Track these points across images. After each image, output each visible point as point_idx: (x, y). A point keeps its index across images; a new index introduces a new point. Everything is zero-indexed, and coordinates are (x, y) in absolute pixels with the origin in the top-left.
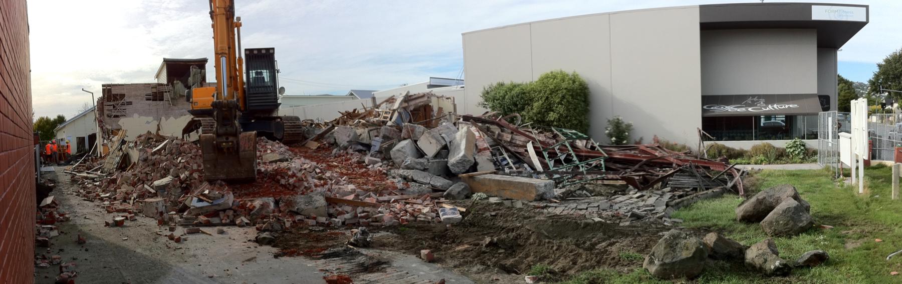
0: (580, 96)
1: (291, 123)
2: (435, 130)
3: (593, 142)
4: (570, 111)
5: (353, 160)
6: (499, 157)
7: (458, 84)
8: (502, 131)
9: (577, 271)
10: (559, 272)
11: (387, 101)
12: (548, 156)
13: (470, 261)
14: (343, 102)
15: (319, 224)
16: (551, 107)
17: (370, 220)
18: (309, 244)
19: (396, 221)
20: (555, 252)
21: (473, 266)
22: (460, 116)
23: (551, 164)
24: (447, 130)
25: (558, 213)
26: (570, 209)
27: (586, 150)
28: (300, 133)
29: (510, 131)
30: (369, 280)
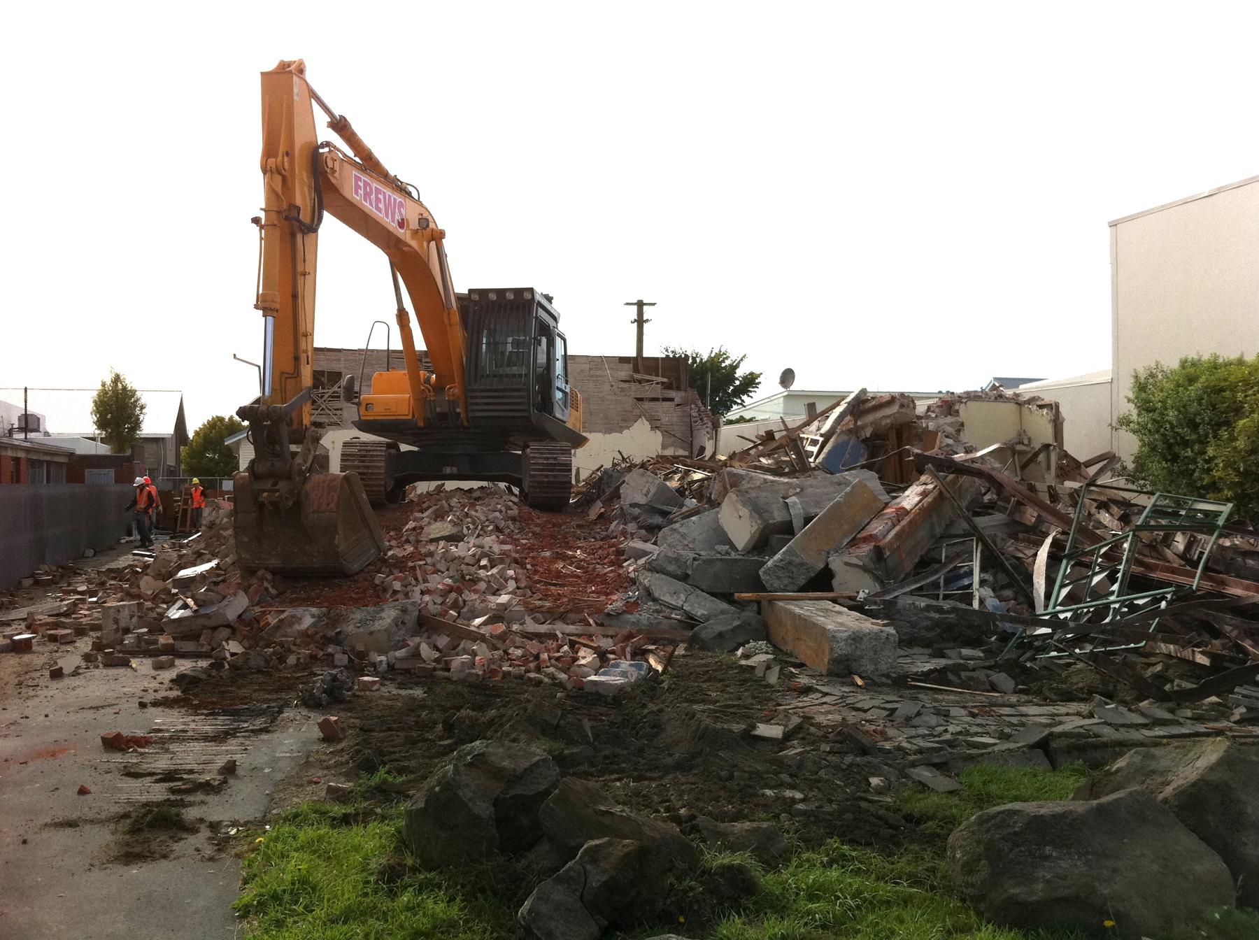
1: (545, 459)
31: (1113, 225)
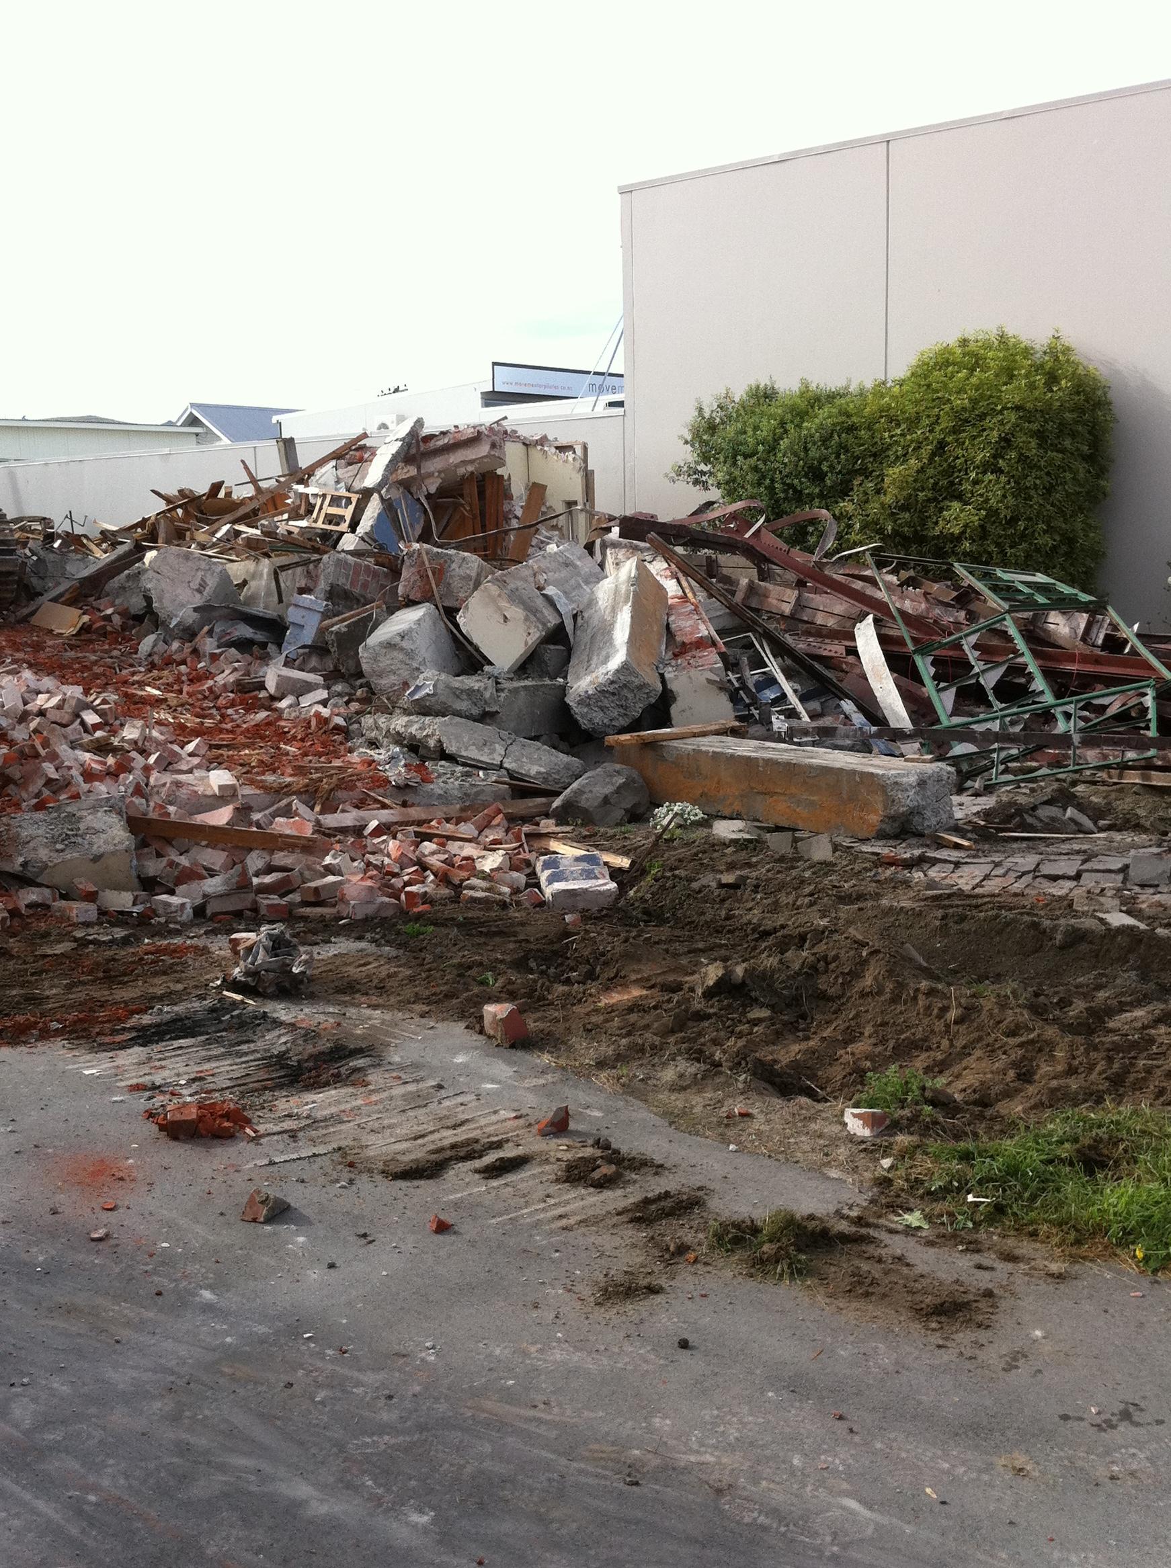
0: (1074, 435)
2: (521, 570)
3: (1117, 619)
4: (1030, 498)
5: (220, 679)
6: (748, 673)
7: (600, 390)
8: (763, 576)
9: (1032, 1108)
10: (967, 1103)
11: (337, 455)
12: (932, 670)
13: (653, 1047)
14: (166, 451)
15: (108, 917)
16: (952, 483)
17: (296, 897)
18: (79, 994)
19: (387, 899)
20: (954, 1028)
21: (664, 1065)
22: (611, 519)
23: (944, 701)
24: (564, 573)
25: (967, 888)
26: (1013, 875)
27: (1087, 650)
28: (10, 573)
29: (791, 576)
30: (308, 1117)
31: (626, 191)
